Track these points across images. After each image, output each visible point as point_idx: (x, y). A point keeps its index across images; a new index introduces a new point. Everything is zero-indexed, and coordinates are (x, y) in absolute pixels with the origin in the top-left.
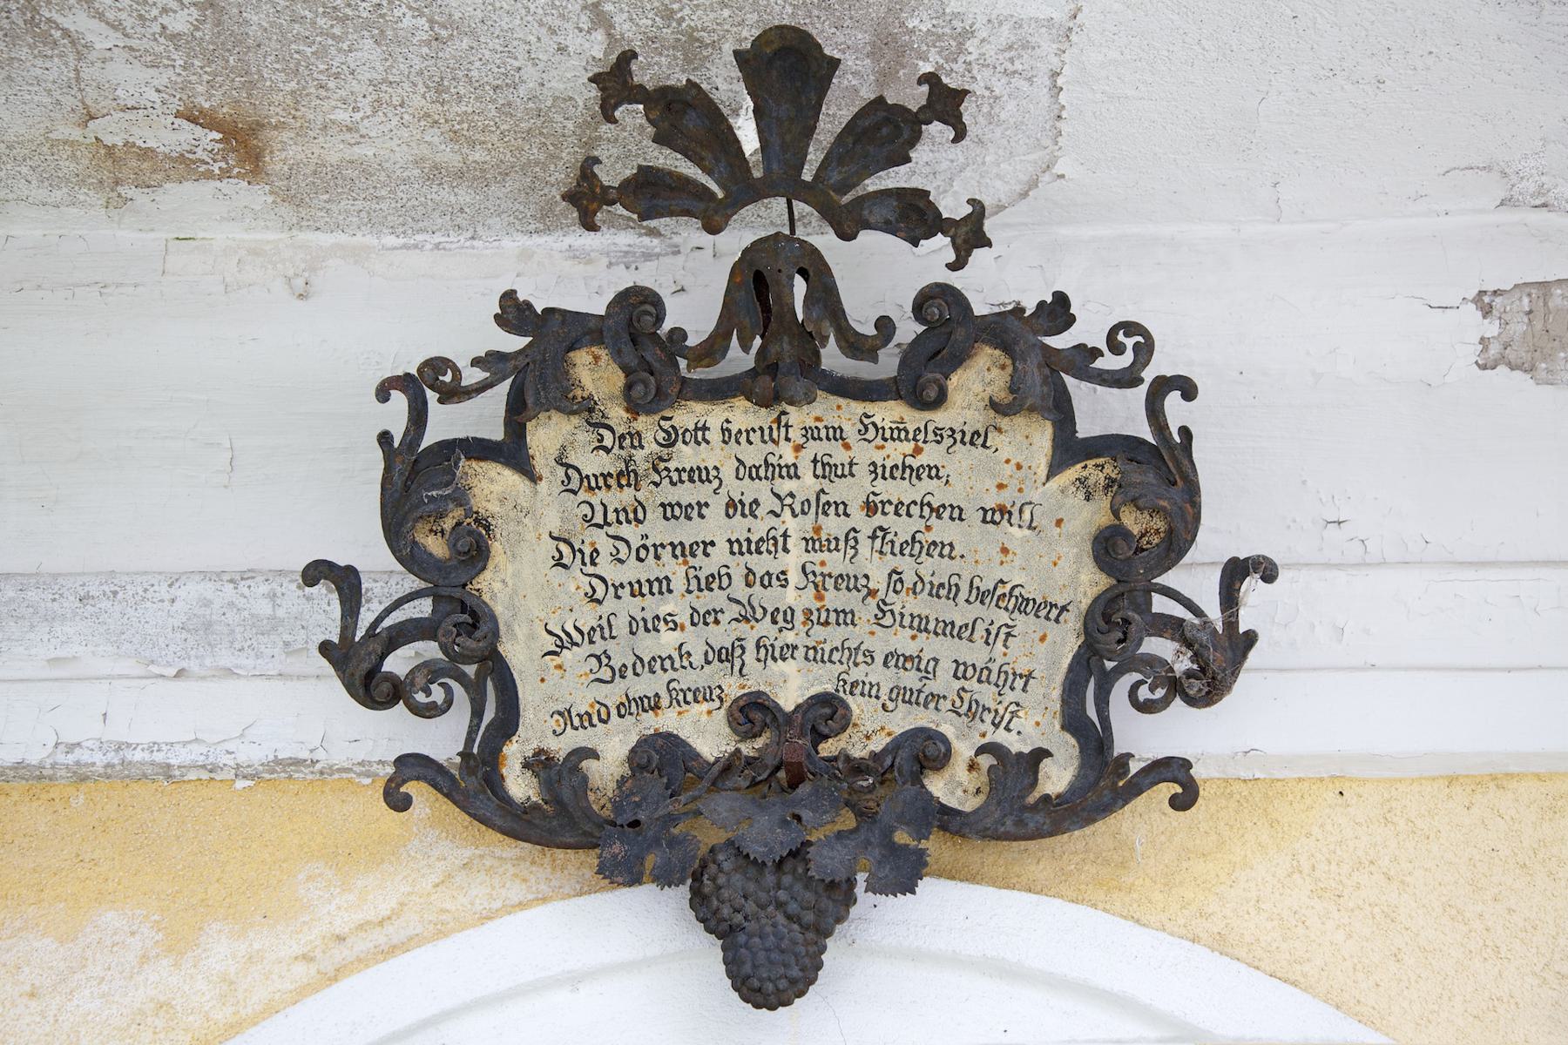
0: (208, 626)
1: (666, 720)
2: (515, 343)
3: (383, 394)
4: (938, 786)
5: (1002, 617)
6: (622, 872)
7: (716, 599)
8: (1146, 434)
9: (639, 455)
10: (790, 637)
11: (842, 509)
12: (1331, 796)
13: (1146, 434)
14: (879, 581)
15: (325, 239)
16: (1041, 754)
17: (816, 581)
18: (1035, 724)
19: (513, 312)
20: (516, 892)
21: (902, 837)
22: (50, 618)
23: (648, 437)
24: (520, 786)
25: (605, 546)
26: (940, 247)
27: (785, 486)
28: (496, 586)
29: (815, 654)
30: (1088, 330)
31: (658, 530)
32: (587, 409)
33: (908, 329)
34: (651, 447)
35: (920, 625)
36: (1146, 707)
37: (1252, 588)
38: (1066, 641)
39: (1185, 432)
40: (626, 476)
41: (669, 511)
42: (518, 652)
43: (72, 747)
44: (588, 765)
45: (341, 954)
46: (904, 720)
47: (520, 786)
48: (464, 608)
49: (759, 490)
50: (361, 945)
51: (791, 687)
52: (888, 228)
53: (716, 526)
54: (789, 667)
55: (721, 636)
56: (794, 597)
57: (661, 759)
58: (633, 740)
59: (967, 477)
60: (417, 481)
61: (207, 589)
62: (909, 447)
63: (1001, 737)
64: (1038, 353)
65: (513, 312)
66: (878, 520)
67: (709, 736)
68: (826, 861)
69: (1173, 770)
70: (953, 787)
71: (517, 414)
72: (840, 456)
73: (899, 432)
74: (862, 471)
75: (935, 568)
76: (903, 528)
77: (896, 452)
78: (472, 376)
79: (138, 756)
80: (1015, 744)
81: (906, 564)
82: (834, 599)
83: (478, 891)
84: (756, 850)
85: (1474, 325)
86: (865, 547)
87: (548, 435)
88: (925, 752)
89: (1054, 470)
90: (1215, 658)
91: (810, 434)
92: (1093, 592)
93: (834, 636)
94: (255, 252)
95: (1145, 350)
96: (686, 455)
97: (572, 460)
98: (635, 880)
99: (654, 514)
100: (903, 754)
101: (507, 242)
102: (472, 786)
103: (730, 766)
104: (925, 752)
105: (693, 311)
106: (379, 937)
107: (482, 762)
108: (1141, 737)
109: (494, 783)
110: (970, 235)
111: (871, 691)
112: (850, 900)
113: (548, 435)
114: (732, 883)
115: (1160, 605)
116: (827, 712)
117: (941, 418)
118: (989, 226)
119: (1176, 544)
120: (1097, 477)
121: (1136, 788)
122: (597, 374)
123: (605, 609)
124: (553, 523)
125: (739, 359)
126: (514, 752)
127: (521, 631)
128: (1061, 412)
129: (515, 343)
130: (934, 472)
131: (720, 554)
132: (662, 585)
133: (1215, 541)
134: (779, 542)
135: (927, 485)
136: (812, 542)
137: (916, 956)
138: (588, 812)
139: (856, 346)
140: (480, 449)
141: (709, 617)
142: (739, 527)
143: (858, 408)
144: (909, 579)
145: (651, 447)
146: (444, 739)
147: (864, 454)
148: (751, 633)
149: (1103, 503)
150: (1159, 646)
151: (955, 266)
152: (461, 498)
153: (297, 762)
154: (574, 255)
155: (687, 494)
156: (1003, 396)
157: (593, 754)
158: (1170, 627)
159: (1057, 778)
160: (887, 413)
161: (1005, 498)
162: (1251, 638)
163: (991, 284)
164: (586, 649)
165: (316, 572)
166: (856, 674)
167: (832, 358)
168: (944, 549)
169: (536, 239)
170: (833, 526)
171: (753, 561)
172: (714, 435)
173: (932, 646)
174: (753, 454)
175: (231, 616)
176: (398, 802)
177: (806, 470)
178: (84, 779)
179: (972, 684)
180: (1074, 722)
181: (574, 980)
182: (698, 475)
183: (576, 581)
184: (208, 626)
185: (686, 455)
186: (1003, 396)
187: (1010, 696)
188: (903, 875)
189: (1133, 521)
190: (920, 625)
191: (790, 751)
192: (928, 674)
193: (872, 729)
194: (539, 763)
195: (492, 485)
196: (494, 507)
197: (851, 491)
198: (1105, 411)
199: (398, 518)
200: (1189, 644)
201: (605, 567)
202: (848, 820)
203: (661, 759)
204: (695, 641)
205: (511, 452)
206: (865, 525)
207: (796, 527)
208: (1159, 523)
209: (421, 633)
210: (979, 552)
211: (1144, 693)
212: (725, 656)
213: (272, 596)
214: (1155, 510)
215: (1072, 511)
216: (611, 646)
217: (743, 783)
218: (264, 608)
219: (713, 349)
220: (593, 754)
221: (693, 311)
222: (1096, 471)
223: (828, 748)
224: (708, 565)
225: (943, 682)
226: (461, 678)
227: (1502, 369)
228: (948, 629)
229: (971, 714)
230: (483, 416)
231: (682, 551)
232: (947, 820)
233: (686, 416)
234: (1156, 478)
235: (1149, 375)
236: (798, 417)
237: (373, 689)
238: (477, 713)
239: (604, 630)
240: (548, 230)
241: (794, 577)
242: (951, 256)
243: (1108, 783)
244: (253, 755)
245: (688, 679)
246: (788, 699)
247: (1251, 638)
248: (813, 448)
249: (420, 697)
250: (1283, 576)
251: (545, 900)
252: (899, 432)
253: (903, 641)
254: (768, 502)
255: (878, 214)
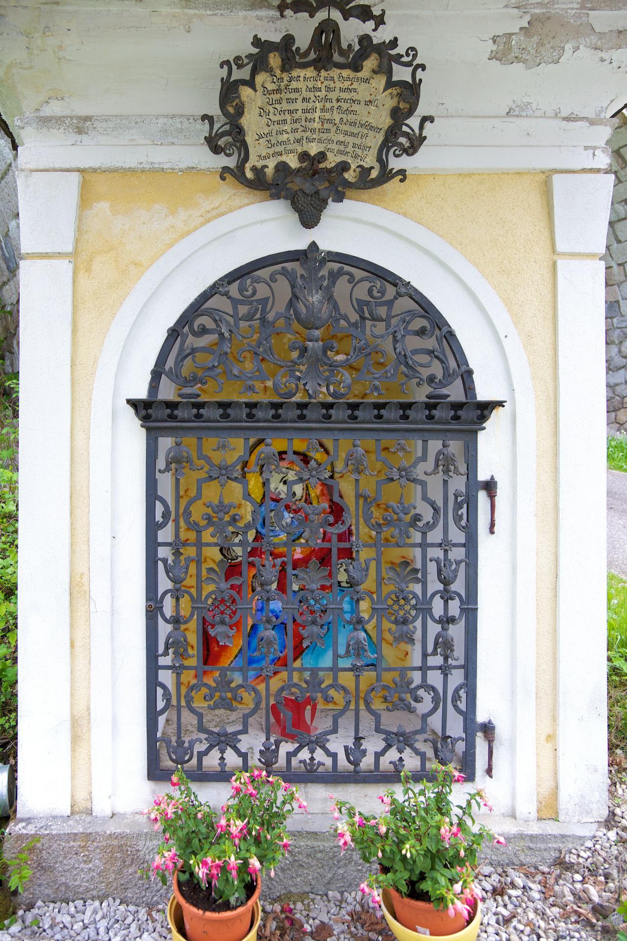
0: (166, 131)
1: (284, 158)
2: (255, 51)
3: (222, 66)
4: (346, 175)
5: (366, 131)
6: (275, 196)
7: (297, 125)
8: (410, 80)
9: (282, 84)
10: (314, 136)
11: (331, 101)
12: (432, 179)
13: (410, 81)
14: (337, 121)
15: (192, 12)
16: (372, 168)
17: (322, 121)
18: (370, 160)
19: (256, 42)
20: (246, 201)
21: (340, 189)
22: (129, 128)
23: (285, 79)
24: (249, 175)
25: (272, 110)
26: (371, 24)
27: (318, 94)
28: (244, 121)
29: (320, 141)
30: (401, 50)
31: (285, 106)
32: (270, 71)
33: (357, 47)
34: (285, 82)
35: (346, 133)
36: (397, 156)
37: (428, 124)
38: (380, 138)
39: (420, 80)
40: (278, 91)
41: (289, 101)
42: (249, 139)
43: (141, 163)
44: (266, 170)
45: (209, 215)
46: (339, 159)
47: (249, 175)
48: (237, 127)
49: (311, 95)
50: (214, 213)
51: (314, 149)
52: (358, 17)
53: (299, 105)
54: (313, 144)
55: (298, 135)
56: (316, 125)
57: (282, 167)
58: (276, 163)
59: (363, 91)
60: (229, 92)
61: (165, 120)
62: (350, 83)
63: (362, 163)
64: (386, 55)
65: (256, 42)
66: (339, 104)
67: (293, 163)
68: (323, 194)
69: (402, 172)
70: (350, 176)
71: (254, 72)
72: (332, 85)
73: (348, 79)
74: (337, 90)
75: (352, 118)
76: (345, 106)
77: (347, 84)
78: (246, 61)
79: (156, 166)
80: (366, 166)
81: (344, 116)
82: (326, 126)
83: (237, 201)
84: (307, 191)
85: (490, 46)
86: (335, 112)
87: (260, 79)
88: (344, 167)
89: (384, 90)
90: (416, 143)
91: (326, 79)
92: (388, 125)
93: (325, 136)
94: (174, 16)
95: (415, 56)
96: (294, 85)
97: (265, 85)
98: (279, 198)
99: (284, 102)
100: (339, 168)
101: (240, 13)
102: (236, 174)
103: (299, 170)
104: (344, 167)
105: (303, 41)
106: (217, 211)
107: (241, 167)
108: (395, 163)
109: (243, 174)
110: (380, 21)
111: (332, 151)
112: (327, 203)
113: (261, 78)
114: (302, 199)
115: (405, 128)
116: (322, 156)
117: (359, 75)
118: (385, 19)
119: (411, 112)
120: (395, 92)
121: (393, 177)
122: (274, 60)
123: (270, 128)
124: (259, 104)
125: (313, 56)
126: (248, 166)
127: (250, 134)
128: (389, 73)
129: (255, 51)
130: (355, 90)
131: (300, 113)
132: (285, 122)
133: (422, 110)
134: (314, 110)
135: (353, 94)
136: (323, 110)
137: (337, 217)
138: (266, 182)
139: (342, 53)
140: (244, 82)
141: (295, 131)
142: (305, 105)
143: (339, 71)
144: (345, 120)
145: (285, 82)
146: (231, 162)
147: (338, 85)
148: (305, 135)
149: (396, 100)
150: (403, 140)
151: (374, 30)
152: (239, 97)
153: (193, 168)
154: (260, 18)
155: (293, 96)
156: (377, 69)
157: (266, 167)
158: (406, 135)
159: (374, 174)
160: (346, 73)
161: (371, 98)
162: (425, 138)
163: (381, 36)
164: (265, 139)
165: (205, 117)
166: (329, 146)
167: (337, 58)
168: (354, 112)
169: (248, 13)
170: (328, 105)
171: (307, 115)
172: (302, 79)
173: (348, 139)
174: (310, 84)
175: (172, 128)
176: (223, 178)
177: (323, 90)
178: (143, 171)
179: (356, 149)
180: (379, 160)
181: (262, 222)
182: (296, 90)
183: (264, 120)
184: (166, 131)
185: (294, 85)
186: (377, 69)
187: (365, 153)
188: (340, 198)
189: (402, 105)
190: (346, 133)
191: (312, 164)
192: (346, 146)
193: (332, 160)
194: (254, 169)
195: (246, 92)
196: (245, 99)
197: (333, 96)
198: (402, 74)
199: (223, 104)
200: (410, 139)
201: (271, 116)
202: (327, 184)
203: (282, 167)
204: (291, 137)
205: (251, 84)
206: (335, 105)
207: (319, 105)
208: (408, 106)
209: (226, 134)
210: (363, 114)
211: (397, 152)
212: (298, 141)
213: (181, 122)
214: (408, 102)
215: (388, 101)
216: (271, 138)
217: (301, 174)
218: (179, 126)
219: (307, 53)
220: (266, 167)
221: (303, 41)
222: (394, 91)
223: (322, 166)
224: (296, 116)
225: (350, 149)
226: (236, 146)
227: (494, 60)
228: (353, 135)
229: (355, 157)
230: (244, 74)
231: (290, 112)
232: (347, 184)
233: (295, 73)
234: (410, 92)
235: (415, 63)
236: (323, 73)
237: (216, 150)
238: (239, 156)
239: (270, 134)
240: (252, 9)
241: (317, 120)
242: (374, 27)
243: (386, 175)
244: (183, 166)
245: (289, 147)
246: (313, 153)
247: (425, 138)
248: (326, 83)
249: (228, 152)
250: (436, 119)
251: (253, 203)
252: (348, 79)
253: (341, 138)
254: (313, 98)
255: (355, 13)
